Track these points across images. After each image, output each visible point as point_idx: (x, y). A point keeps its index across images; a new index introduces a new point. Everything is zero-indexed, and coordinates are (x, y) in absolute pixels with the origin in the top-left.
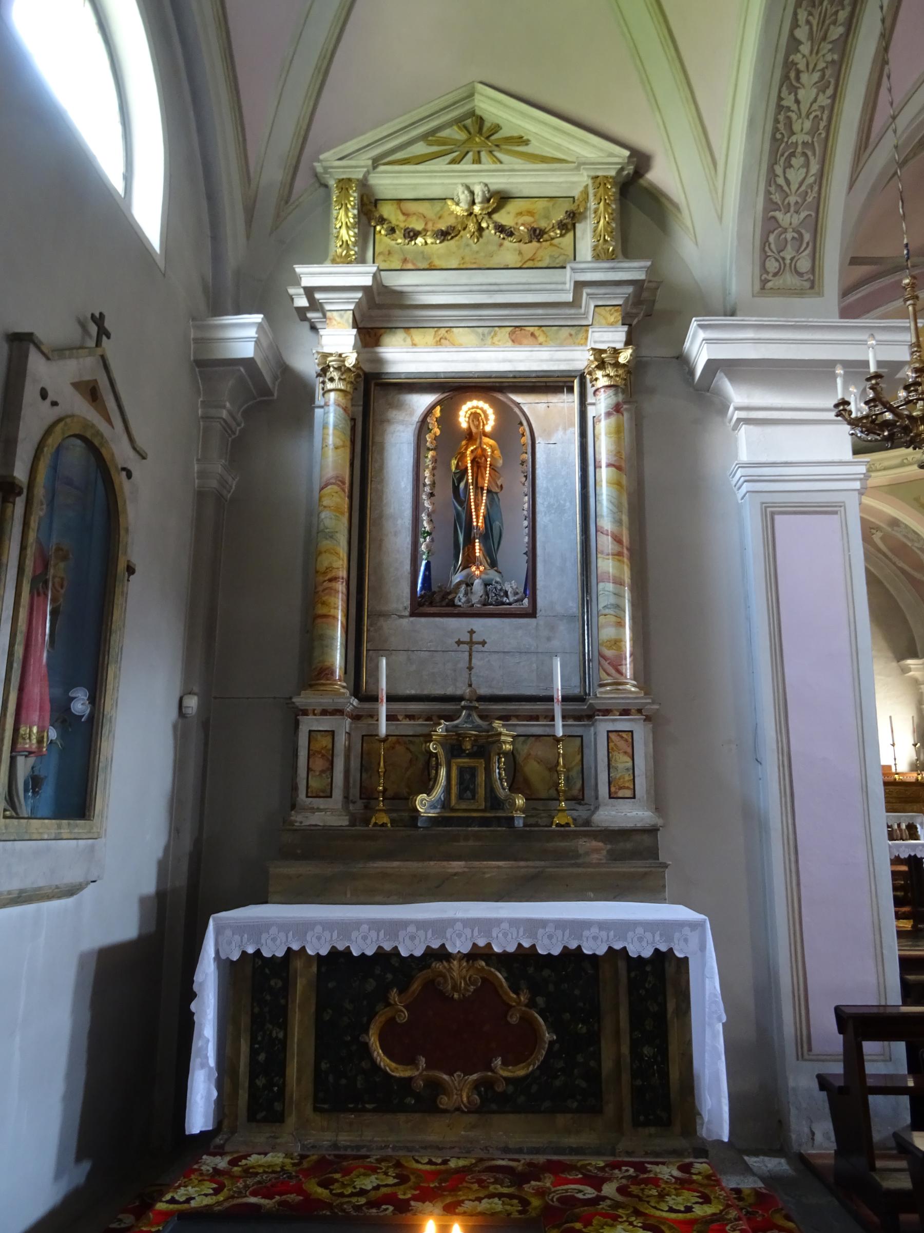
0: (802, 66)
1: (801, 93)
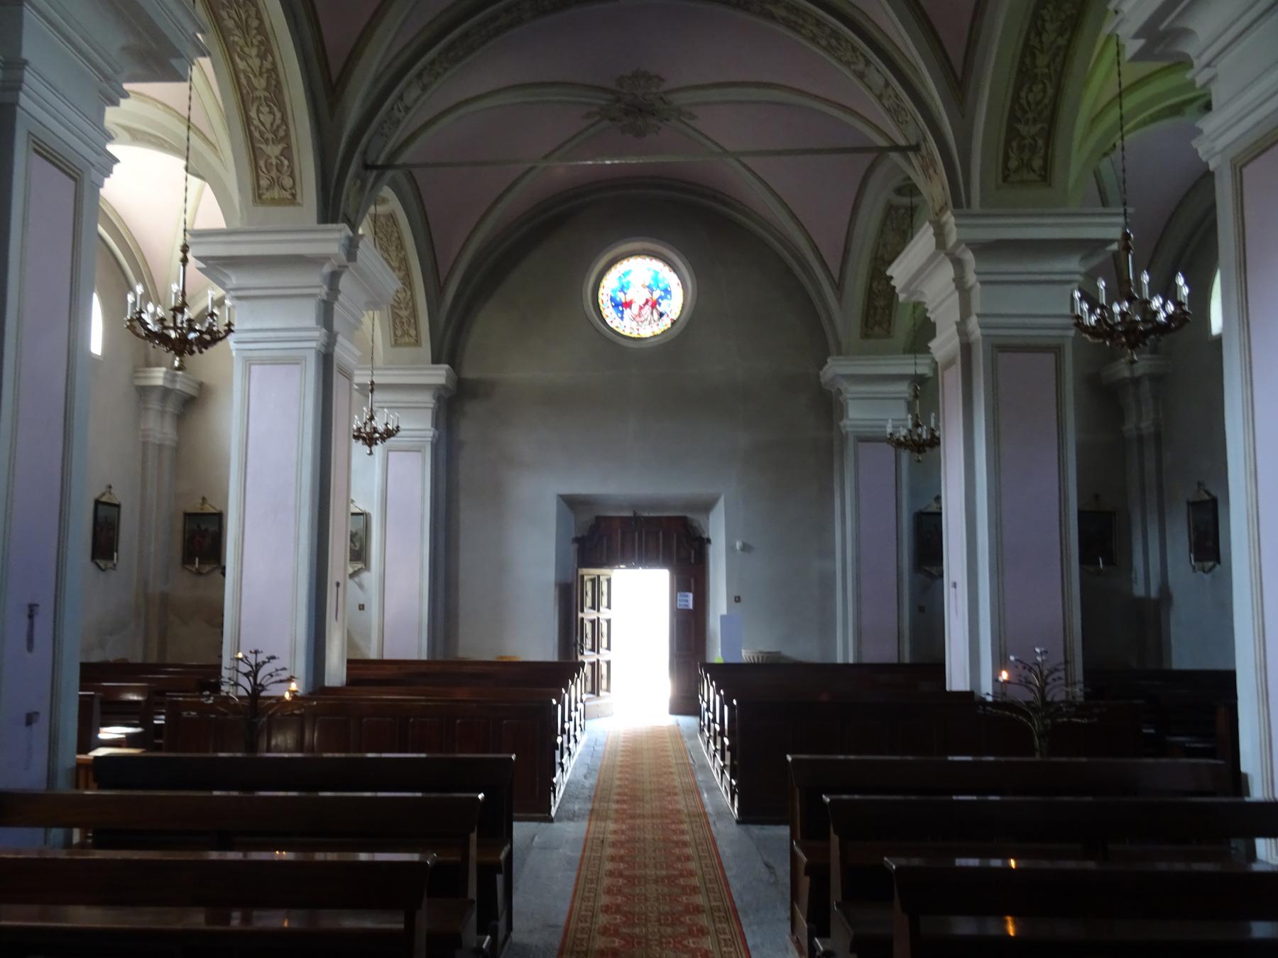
0: (1047, 18)
1: (1045, 38)
